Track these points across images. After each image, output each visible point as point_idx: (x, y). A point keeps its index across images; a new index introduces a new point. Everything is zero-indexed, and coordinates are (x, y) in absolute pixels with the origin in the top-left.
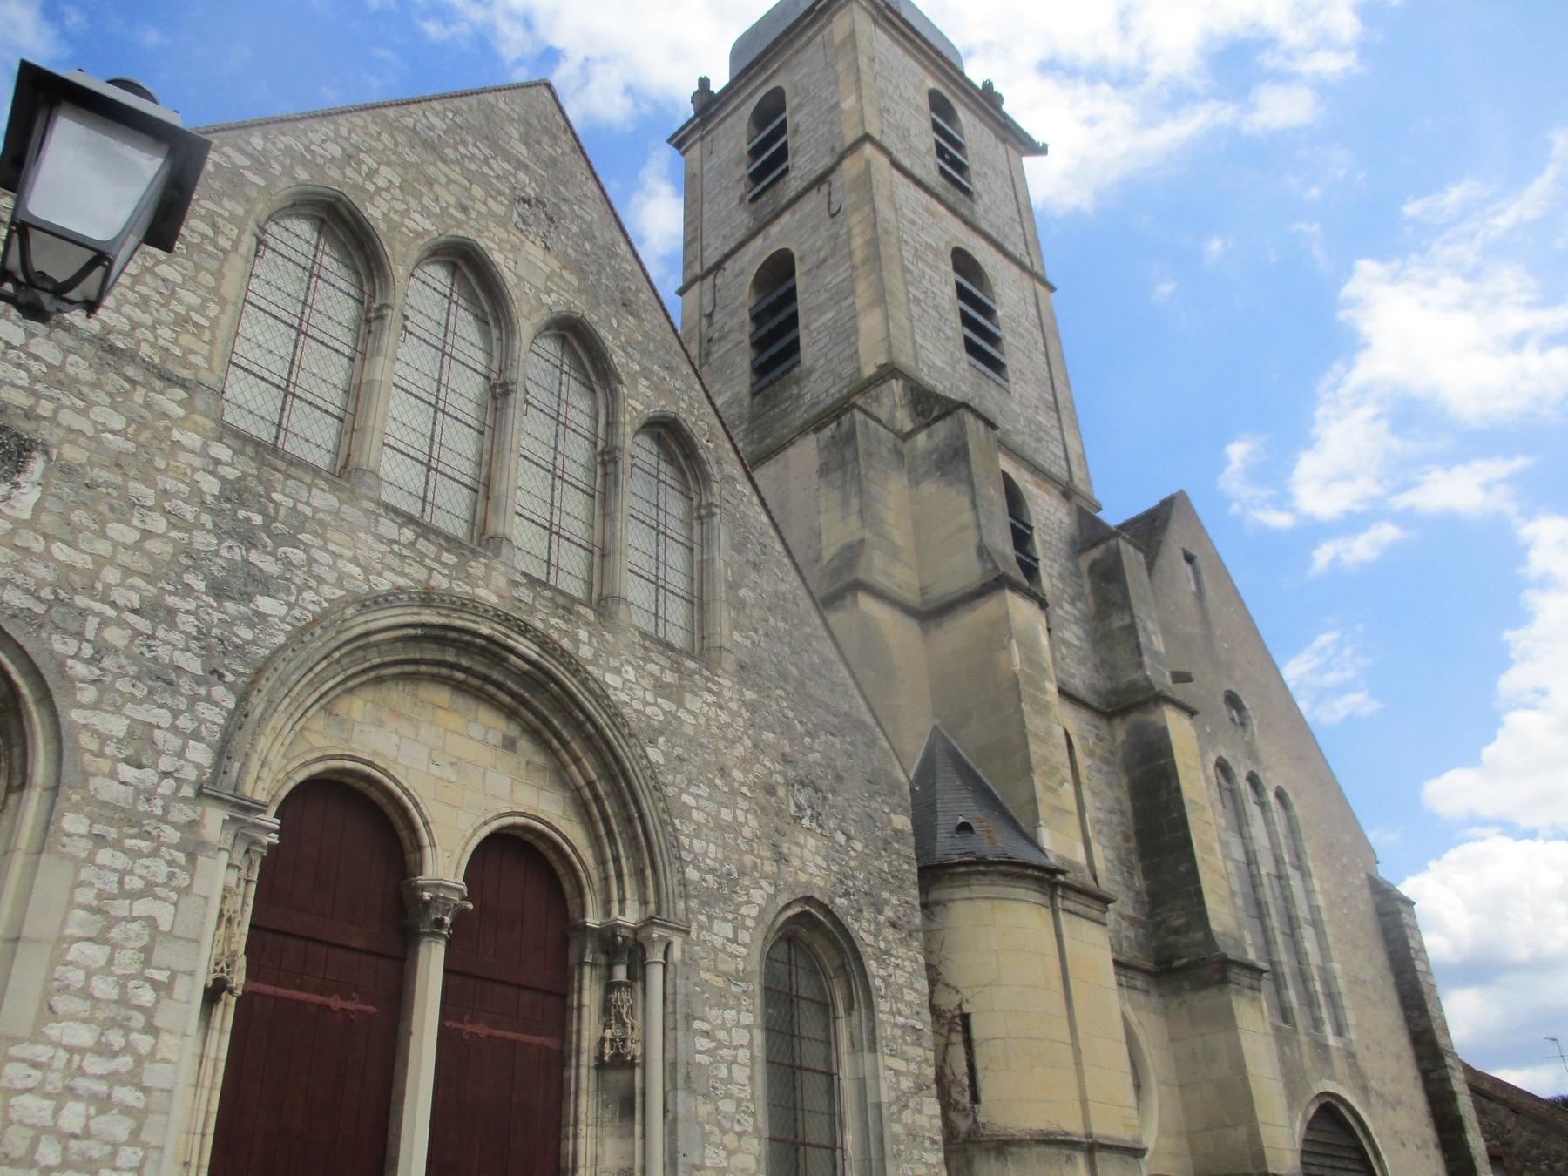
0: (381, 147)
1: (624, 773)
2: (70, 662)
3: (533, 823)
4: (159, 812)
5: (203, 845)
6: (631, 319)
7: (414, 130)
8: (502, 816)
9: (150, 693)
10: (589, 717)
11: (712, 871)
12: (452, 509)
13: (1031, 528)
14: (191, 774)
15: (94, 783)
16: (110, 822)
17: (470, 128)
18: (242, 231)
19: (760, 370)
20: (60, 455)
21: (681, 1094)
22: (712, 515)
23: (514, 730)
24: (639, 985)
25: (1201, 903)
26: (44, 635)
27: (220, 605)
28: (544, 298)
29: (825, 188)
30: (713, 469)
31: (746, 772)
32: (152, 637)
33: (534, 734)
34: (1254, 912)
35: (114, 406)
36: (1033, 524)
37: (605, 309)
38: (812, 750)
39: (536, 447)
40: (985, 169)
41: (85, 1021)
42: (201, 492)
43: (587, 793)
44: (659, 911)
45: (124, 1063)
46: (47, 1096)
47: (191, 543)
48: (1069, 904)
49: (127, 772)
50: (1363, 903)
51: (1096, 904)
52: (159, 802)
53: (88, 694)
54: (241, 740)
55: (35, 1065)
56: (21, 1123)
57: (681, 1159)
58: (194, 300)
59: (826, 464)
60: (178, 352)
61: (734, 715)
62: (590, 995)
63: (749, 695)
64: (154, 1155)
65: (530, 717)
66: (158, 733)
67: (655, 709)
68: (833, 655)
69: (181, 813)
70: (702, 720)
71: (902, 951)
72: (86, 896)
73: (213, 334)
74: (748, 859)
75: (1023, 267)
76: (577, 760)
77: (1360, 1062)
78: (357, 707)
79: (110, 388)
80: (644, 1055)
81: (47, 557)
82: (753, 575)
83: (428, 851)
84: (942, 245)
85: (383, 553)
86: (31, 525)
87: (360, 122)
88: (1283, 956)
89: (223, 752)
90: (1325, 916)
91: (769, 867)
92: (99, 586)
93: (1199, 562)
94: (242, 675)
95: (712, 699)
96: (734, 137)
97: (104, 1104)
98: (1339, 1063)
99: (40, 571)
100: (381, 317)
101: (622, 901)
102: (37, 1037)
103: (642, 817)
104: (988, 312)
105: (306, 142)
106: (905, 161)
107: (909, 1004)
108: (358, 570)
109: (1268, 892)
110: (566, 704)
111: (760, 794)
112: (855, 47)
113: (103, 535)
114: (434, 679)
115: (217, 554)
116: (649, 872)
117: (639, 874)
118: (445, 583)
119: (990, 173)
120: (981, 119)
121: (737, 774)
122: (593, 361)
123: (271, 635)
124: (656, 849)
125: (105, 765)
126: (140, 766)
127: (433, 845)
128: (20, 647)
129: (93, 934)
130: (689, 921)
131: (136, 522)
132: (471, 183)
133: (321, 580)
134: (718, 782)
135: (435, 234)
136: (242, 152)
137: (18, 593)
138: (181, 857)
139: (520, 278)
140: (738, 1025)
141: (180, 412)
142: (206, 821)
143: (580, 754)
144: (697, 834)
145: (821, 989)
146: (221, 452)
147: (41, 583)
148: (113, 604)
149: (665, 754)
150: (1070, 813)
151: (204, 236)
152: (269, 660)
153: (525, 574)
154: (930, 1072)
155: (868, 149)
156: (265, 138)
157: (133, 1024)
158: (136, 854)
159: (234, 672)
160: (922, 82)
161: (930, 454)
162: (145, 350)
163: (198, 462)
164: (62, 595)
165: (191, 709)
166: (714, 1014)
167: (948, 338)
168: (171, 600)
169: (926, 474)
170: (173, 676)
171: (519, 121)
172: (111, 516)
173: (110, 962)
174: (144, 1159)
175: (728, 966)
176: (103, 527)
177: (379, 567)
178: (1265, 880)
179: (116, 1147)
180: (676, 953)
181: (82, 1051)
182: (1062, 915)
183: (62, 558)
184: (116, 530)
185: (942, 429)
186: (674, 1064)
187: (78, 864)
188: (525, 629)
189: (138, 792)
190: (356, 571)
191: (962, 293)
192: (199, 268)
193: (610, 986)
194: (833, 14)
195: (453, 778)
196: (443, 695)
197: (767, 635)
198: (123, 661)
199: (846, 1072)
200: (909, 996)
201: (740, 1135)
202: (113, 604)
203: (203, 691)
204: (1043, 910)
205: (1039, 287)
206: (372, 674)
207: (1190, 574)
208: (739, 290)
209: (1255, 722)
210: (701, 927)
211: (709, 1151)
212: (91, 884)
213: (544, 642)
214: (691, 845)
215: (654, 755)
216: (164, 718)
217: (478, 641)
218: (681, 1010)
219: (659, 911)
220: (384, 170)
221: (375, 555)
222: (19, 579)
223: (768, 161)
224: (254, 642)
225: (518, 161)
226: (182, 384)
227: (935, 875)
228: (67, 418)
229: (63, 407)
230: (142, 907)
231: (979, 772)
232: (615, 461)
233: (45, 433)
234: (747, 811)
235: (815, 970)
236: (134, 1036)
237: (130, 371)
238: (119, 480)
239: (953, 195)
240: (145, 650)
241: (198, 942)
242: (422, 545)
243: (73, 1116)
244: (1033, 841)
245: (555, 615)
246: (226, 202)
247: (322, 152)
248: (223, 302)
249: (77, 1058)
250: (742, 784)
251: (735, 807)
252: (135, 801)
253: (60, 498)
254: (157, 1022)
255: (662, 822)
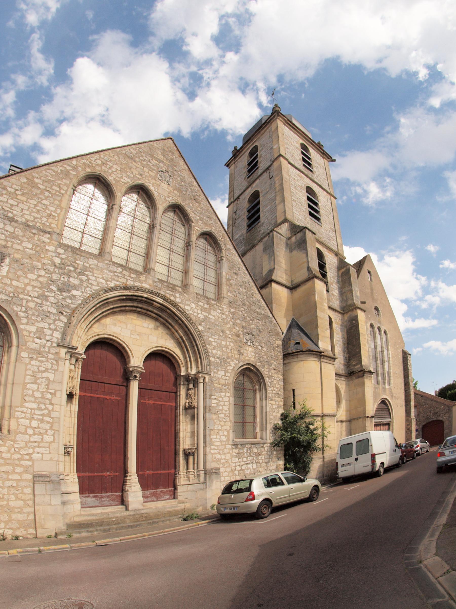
0: (114, 159)
1: (191, 333)
2: (19, 313)
3: (164, 349)
4: (47, 350)
5: (60, 358)
6: (197, 204)
7: (126, 154)
8: (154, 347)
9: (42, 319)
10: (180, 319)
11: (218, 358)
12: (137, 262)
13: (325, 264)
14: (55, 340)
15: (28, 344)
16: (34, 354)
17: (144, 152)
18: (68, 188)
19: (249, 226)
20: (13, 257)
21: (207, 414)
22: (222, 260)
23: (158, 324)
24: (196, 389)
25: (361, 358)
26: (11, 306)
27: (61, 294)
28: (168, 199)
29: (268, 171)
30: (223, 246)
31: (230, 331)
32: (42, 304)
33: (164, 325)
34: (374, 360)
35: (29, 241)
36: (326, 263)
37: (188, 201)
38: (252, 324)
39: (165, 243)
40: (317, 165)
41: (34, 402)
42: (55, 263)
43: (180, 340)
44: (202, 369)
45: (46, 412)
46: (27, 419)
47: (52, 277)
48: (324, 360)
49: (37, 341)
50: (400, 356)
51: (332, 360)
52: (47, 348)
53: (25, 321)
54: (69, 331)
55: (22, 412)
56: (22, 425)
57: (207, 428)
58: (52, 209)
59: (265, 248)
60: (48, 224)
61: (227, 316)
62: (183, 392)
63: (232, 310)
64: (56, 432)
65: (162, 320)
66: (45, 330)
67: (201, 315)
68: (260, 298)
69: (53, 351)
70: (217, 318)
71: (276, 375)
72: (29, 372)
73: (58, 218)
74: (230, 355)
75: (327, 192)
76: (177, 331)
77: (392, 391)
78: (108, 321)
79: (28, 237)
80: (198, 405)
81: (11, 285)
82: (235, 276)
83: (131, 358)
84: (303, 185)
85: (112, 276)
86: (7, 277)
87: (108, 153)
88: (380, 370)
89: (64, 334)
90: (391, 359)
91: (237, 356)
92: (26, 292)
93: (372, 273)
94: (68, 312)
95: (220, 311)
96: (244, 159)
97: (42, 421)
98: (388, 392)
99: (9, 289)
100: (112, 208)
101: (191, 368)
102: (22, 406)
103: (197, 345)
104: (316, 204)
105: (90, 160)
106: (293, 163)
107: (278, 388)
108: (104, 281)
109: (379, 355)
110: (172, 315)
111: (235, 338)
112: (278, 131)
113: (26, 277)
114: (131, 311)
115: (60, 280)
116: (199, 360)
117: (196, 360)
118: (132, 283)
119: (319, 166)
120: (316, 152)
121: (228, 332)
122: (184, 217)
123: (77, 301)
124: (201, 353)
125: (31, 339)
126: (41, 339)
127: (133, 356)
128: (5, 310)
129: (33, 382)
130: (211, 371)
131: (36, 273)
132: (144, 167)
133: (92, 284)
134: (221, 334)
135: (131, 183)
136: (69, 165)
137: (4, 295)
138: (54, 362)
139: (159, 194)
140: (225, 396)
141: (48, 241)
142: (61, 352)
143: (178, 329)
144: (214, 349)
145: (253, 387)
146: (61, 251)
147: (10, 292)
148: (30, 296)
149: (204, 327)
150: (328, 337)
151: (56, 191)
152: (76, 308)
153: (158, 279)
154: (282, 403)
155: (281, 158)
156: (77, 161)
157: (46, 403)
158: (42, 362)
159: (66, 312)
160: (299, 141)
161: (296, 243)
162: (38, 224)
163: (54, 254)
164: (16, 295)
165: (54, 323)
166: (218, 395)
167: (304, 211)
168: (47, 294)
169: (294, 249)
170: (48, 314)
171: (161, 149)
172: (29, 272)
173: (38, 388)
174: (54, 433)
175: (222, 382)
176: (26, 276)
177: (110, 279)
178: (378, 352)
179: (47, 431)
180: (207, 380)
181: (34, 409)
182: (322, 363)
183: (15, 285)
184: (30, 276)
185: (299, 235)
186: (206, 407)
187: (26, 365)
188: (158, 295)
189: (41, 346)
190: (103, 281)
191: (309, 199)
192: (55, 200)
193: (188, 389)
194: (272, 123)
195: (138, 338)
196: (136, 315)
197: (239, 293)
198: (34, 311)
199: (258, 405)
200: (277, 386)
201: (225, 422)
202: (30, 296)
203: (57, 318)
204: (317, 362)
205: (332, 198)
206: (111, 311)
207: (369, 277)
208: (244, 204)
209: (381, 314)
210: (215, 373)
211: (216, 426)
212: (30, 370)
213: (165, 299)
214: (212, 351)
215: (200, 328)
216: (47, 326)
217: (143, 299)
218: (208, 394)
219: (202, 369)
220: (115, 166)
221: (109, 276)
222: (4, 291)
223: (253, 166)
224: (72, 303)
225: (160, 160)
226: (49, 233)
227: (287, 356)
228: (16, 246)
229: (15, 243)
230: (45, 375)
231: (304, 329)
232: (190, 245)
233: (9, 251)
234: (230, 342)
235: (251, 382)
236: (47, 406)
237: (34, 231)
238: (31, 262)
239: (307, 172)
240: (40, 308)
241: (61, 383)
242: (124, 272)
243: (35, 424)
244: (317, 345)
245: (168, 290)
246: (64, 180)
247: (95, 163)
248: (62, 209)
249: (33, 411)
250: (229, 335)
251: (227, 340)
252: (40, 348)
253: (14, 269)
254: (53, 402)
255: (203, 346)
